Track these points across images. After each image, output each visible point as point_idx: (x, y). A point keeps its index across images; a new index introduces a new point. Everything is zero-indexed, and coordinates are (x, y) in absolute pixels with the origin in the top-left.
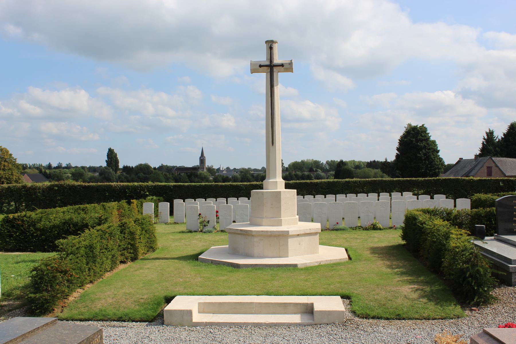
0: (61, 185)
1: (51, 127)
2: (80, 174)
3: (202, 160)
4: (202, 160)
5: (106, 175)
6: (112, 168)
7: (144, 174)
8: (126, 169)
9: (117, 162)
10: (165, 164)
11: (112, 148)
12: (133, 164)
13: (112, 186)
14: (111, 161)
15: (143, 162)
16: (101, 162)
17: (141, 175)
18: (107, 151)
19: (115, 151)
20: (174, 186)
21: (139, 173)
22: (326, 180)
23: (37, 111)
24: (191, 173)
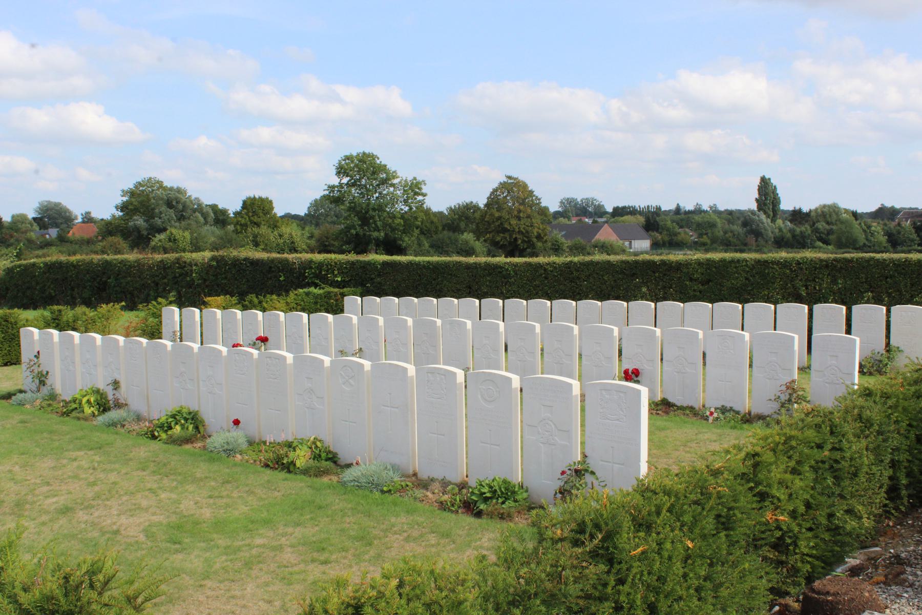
0: (223, 257)
1: (697, 141)
2: (709, 223)
5: (754, 227)
6: (765, 213)
7: (828, 223)
8: (797, 216)
9: (776, 201)
10: (888, 204)
11: (767, 177)
12: (807, 205)
13: (287, 260)
14: (766, 199)
15: (829, 202)
16: (747, 201)
17: (820, 227)
18: (757, 182)
19: (774, 181)
20: (385, 264)
21: (818, 221)
22: (699, 256)
23: (676, 113)
24: (738, 229)
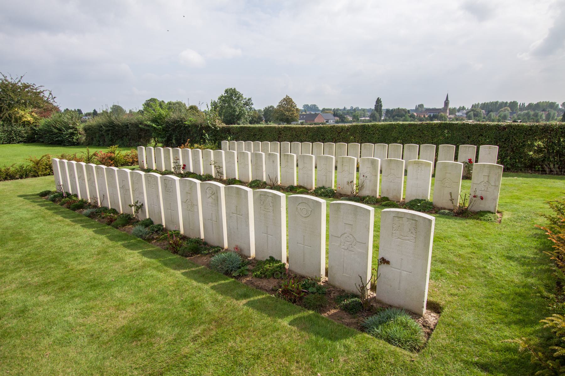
3: (446, 103)
4: (446, 103)
